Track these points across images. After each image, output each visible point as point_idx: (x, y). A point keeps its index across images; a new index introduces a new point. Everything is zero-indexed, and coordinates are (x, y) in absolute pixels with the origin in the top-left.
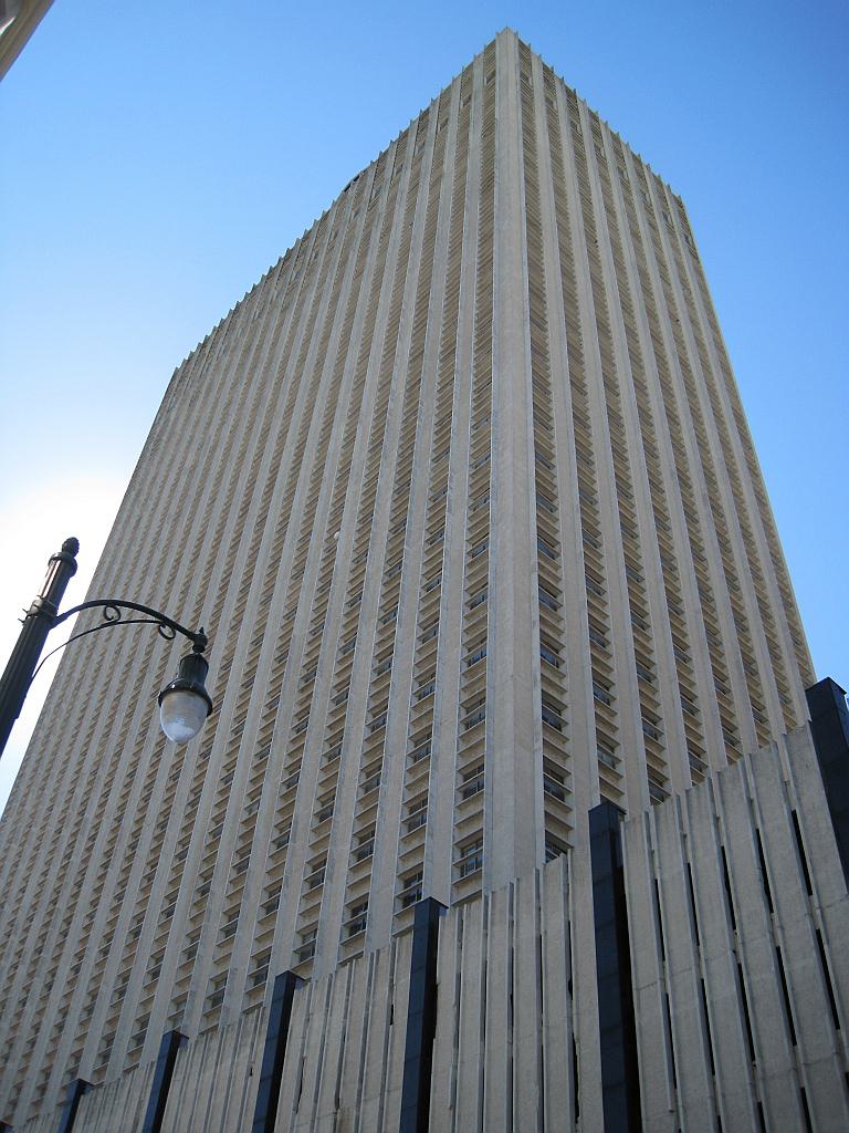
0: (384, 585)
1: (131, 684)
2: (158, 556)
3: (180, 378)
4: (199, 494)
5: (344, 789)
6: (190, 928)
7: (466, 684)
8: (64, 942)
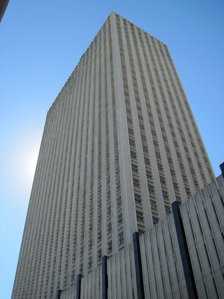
0: (98, 169)
1: (47, 197)
2: (49, 163)
3: (49, 113)
4: (57, 146)
5: (95, 222)
6: (89, 239)
7: (117, 194)
8: (40, 265)
